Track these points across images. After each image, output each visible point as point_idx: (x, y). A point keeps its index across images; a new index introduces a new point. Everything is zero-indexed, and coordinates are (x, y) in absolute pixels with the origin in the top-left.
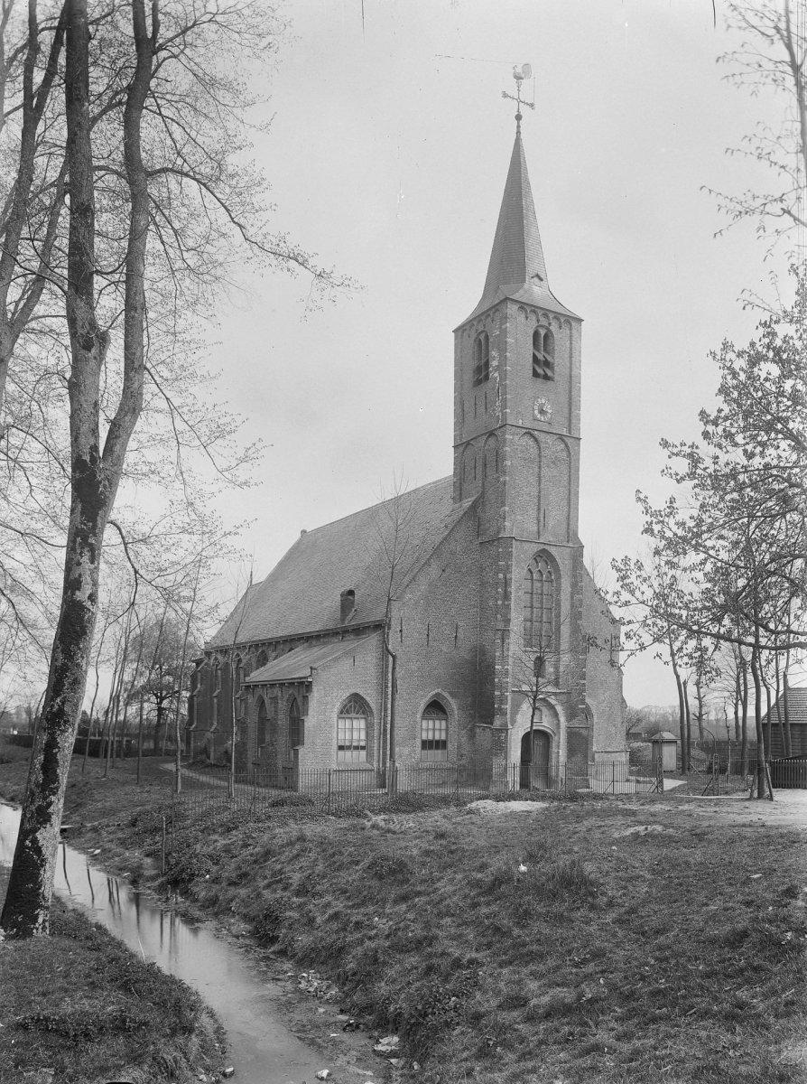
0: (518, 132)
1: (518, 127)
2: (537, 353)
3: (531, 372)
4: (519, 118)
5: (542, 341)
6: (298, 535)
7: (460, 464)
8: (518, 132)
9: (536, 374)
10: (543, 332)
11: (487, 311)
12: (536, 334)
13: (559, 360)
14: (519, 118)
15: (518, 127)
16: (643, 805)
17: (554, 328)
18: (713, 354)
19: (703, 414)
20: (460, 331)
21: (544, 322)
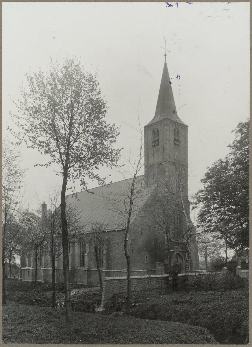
0: (165, 60)
1: (165, 58)
2: (175, 137)
3: (173, 144)
4: (165, 55)
5: (176, 133)
6: (230, 3)
7: (148, 167)
8: (165, 60)
9: (175, 144)
10: (177, 130)
11: (156, 123)
12: (175, 131)
13: (182, 139)
14: (165, 55)
15: (165, 58)
16: (186, 217)
17: (180, 129)
18: (109, 124)
19: (105, 117)
20: (147, 128)
21: (177, 127)
